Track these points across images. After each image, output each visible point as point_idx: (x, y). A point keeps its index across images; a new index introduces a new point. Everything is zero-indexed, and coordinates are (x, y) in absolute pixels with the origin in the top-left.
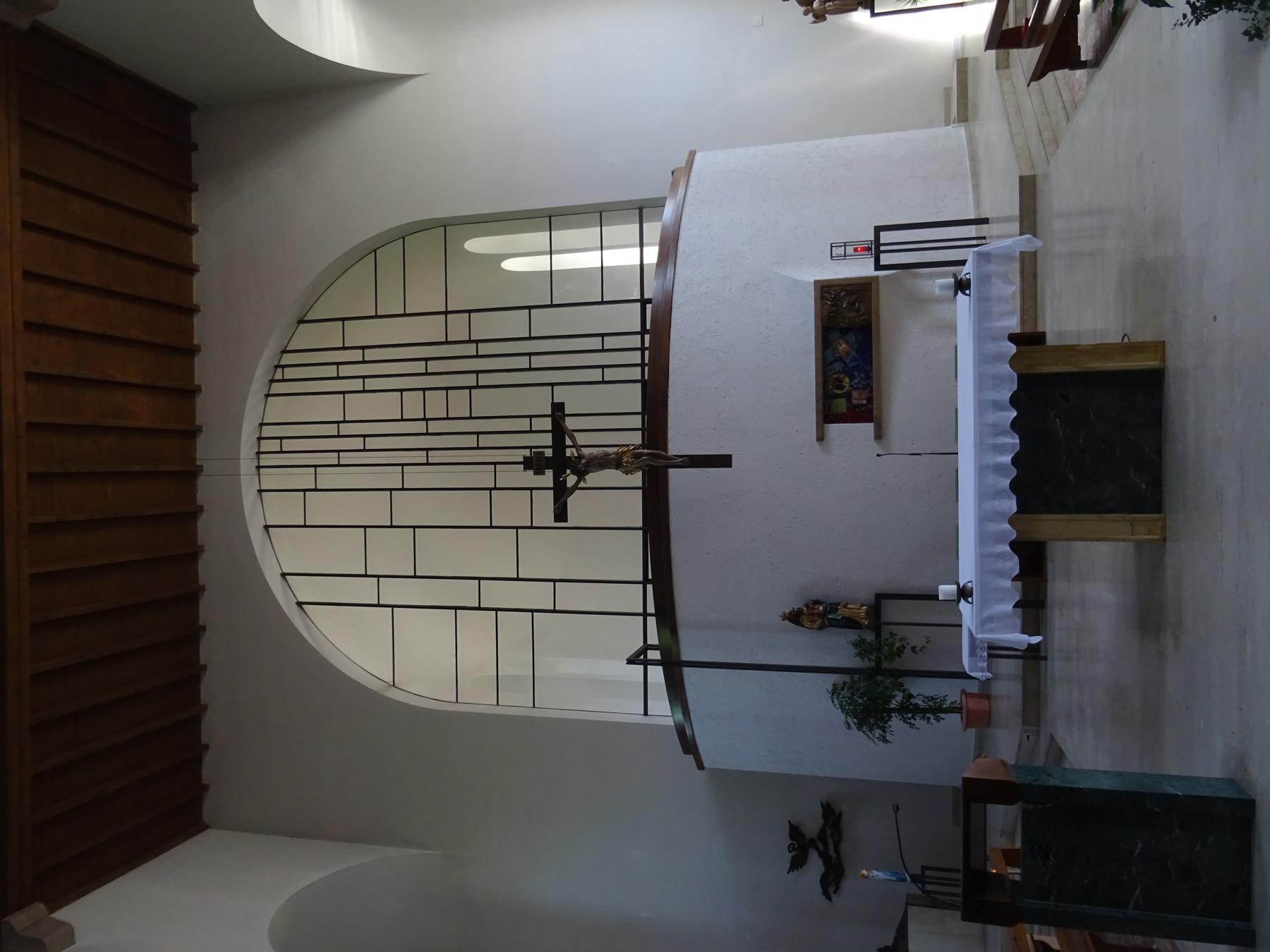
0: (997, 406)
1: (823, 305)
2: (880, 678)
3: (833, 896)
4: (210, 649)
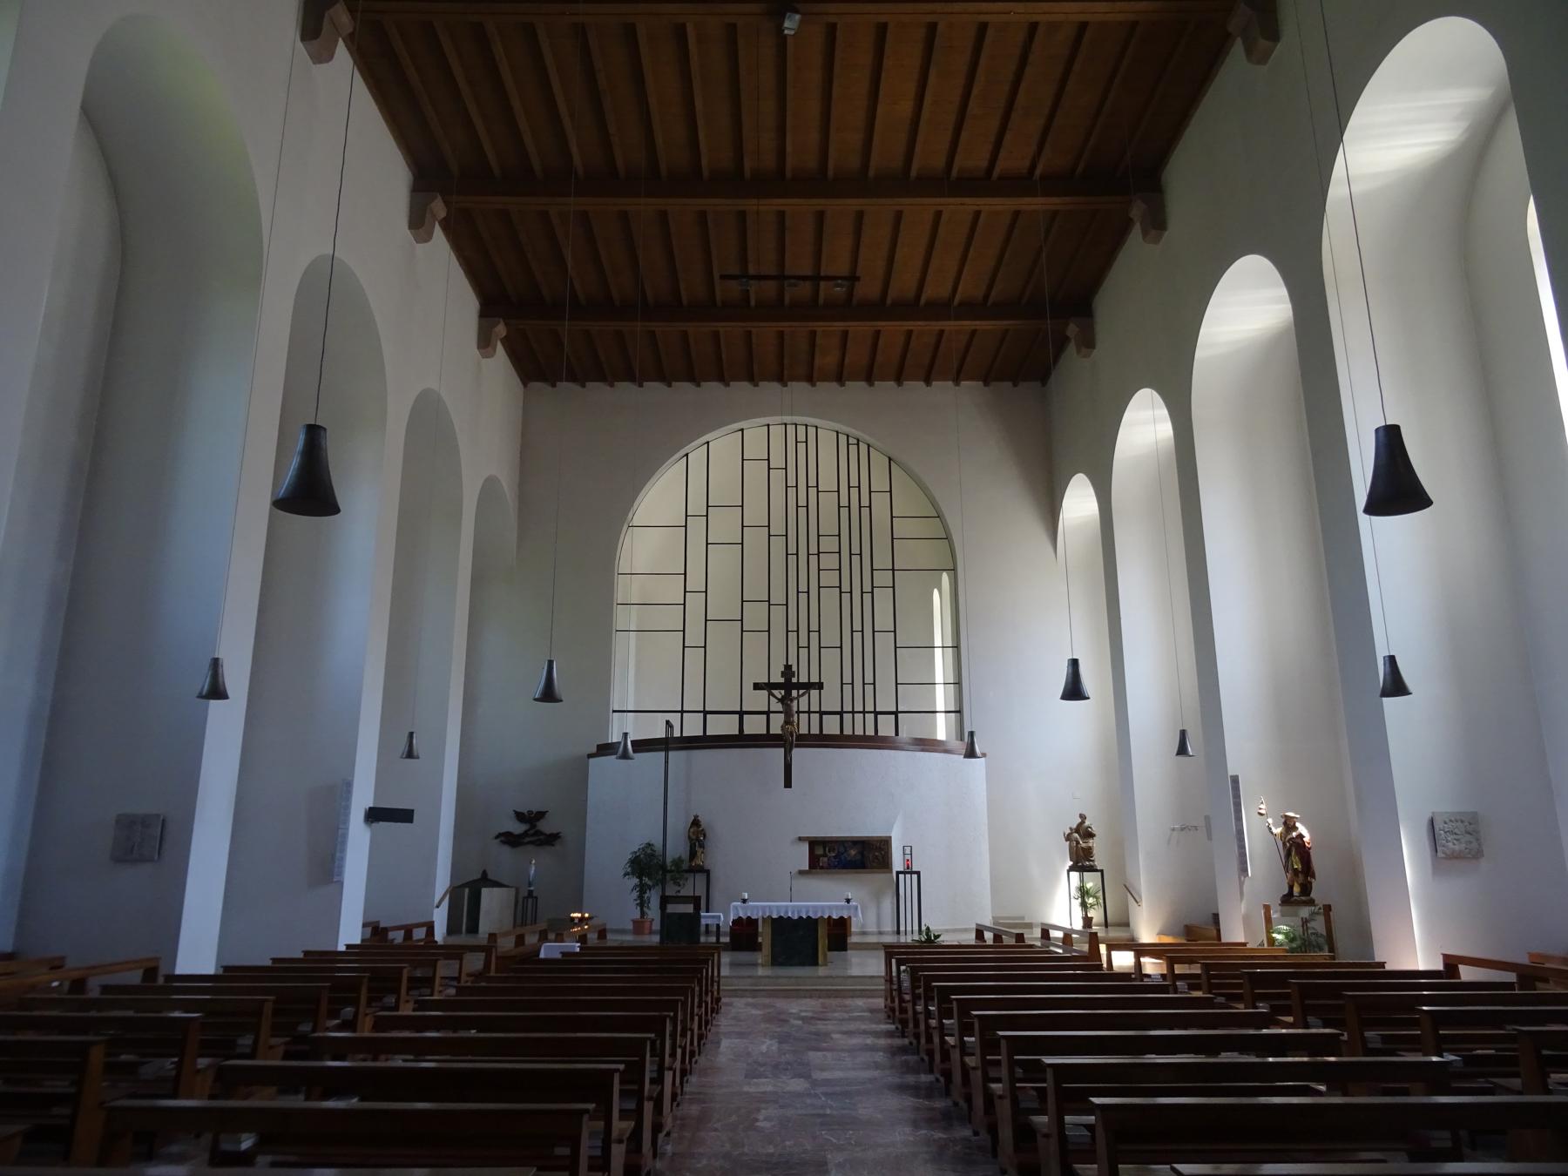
0: (807, 912)
1: (877, 841)
2: (661, 872)
3: (498, 840)
4: (655, 390)
